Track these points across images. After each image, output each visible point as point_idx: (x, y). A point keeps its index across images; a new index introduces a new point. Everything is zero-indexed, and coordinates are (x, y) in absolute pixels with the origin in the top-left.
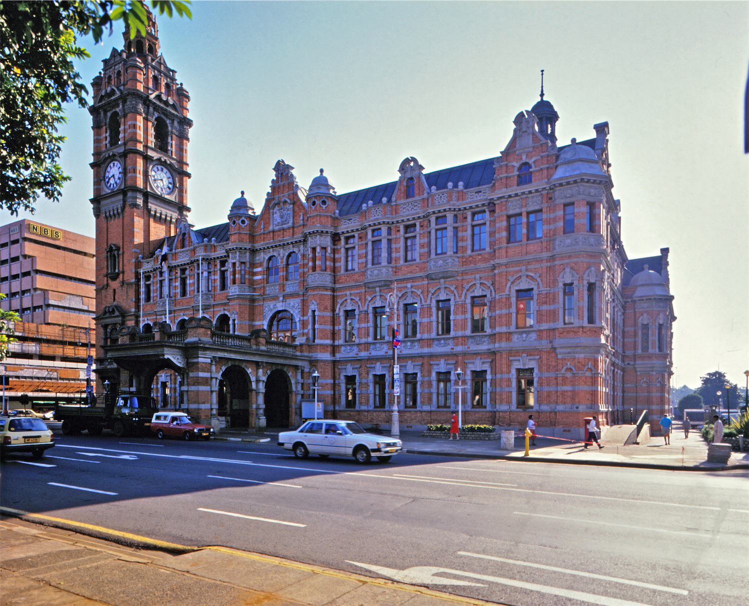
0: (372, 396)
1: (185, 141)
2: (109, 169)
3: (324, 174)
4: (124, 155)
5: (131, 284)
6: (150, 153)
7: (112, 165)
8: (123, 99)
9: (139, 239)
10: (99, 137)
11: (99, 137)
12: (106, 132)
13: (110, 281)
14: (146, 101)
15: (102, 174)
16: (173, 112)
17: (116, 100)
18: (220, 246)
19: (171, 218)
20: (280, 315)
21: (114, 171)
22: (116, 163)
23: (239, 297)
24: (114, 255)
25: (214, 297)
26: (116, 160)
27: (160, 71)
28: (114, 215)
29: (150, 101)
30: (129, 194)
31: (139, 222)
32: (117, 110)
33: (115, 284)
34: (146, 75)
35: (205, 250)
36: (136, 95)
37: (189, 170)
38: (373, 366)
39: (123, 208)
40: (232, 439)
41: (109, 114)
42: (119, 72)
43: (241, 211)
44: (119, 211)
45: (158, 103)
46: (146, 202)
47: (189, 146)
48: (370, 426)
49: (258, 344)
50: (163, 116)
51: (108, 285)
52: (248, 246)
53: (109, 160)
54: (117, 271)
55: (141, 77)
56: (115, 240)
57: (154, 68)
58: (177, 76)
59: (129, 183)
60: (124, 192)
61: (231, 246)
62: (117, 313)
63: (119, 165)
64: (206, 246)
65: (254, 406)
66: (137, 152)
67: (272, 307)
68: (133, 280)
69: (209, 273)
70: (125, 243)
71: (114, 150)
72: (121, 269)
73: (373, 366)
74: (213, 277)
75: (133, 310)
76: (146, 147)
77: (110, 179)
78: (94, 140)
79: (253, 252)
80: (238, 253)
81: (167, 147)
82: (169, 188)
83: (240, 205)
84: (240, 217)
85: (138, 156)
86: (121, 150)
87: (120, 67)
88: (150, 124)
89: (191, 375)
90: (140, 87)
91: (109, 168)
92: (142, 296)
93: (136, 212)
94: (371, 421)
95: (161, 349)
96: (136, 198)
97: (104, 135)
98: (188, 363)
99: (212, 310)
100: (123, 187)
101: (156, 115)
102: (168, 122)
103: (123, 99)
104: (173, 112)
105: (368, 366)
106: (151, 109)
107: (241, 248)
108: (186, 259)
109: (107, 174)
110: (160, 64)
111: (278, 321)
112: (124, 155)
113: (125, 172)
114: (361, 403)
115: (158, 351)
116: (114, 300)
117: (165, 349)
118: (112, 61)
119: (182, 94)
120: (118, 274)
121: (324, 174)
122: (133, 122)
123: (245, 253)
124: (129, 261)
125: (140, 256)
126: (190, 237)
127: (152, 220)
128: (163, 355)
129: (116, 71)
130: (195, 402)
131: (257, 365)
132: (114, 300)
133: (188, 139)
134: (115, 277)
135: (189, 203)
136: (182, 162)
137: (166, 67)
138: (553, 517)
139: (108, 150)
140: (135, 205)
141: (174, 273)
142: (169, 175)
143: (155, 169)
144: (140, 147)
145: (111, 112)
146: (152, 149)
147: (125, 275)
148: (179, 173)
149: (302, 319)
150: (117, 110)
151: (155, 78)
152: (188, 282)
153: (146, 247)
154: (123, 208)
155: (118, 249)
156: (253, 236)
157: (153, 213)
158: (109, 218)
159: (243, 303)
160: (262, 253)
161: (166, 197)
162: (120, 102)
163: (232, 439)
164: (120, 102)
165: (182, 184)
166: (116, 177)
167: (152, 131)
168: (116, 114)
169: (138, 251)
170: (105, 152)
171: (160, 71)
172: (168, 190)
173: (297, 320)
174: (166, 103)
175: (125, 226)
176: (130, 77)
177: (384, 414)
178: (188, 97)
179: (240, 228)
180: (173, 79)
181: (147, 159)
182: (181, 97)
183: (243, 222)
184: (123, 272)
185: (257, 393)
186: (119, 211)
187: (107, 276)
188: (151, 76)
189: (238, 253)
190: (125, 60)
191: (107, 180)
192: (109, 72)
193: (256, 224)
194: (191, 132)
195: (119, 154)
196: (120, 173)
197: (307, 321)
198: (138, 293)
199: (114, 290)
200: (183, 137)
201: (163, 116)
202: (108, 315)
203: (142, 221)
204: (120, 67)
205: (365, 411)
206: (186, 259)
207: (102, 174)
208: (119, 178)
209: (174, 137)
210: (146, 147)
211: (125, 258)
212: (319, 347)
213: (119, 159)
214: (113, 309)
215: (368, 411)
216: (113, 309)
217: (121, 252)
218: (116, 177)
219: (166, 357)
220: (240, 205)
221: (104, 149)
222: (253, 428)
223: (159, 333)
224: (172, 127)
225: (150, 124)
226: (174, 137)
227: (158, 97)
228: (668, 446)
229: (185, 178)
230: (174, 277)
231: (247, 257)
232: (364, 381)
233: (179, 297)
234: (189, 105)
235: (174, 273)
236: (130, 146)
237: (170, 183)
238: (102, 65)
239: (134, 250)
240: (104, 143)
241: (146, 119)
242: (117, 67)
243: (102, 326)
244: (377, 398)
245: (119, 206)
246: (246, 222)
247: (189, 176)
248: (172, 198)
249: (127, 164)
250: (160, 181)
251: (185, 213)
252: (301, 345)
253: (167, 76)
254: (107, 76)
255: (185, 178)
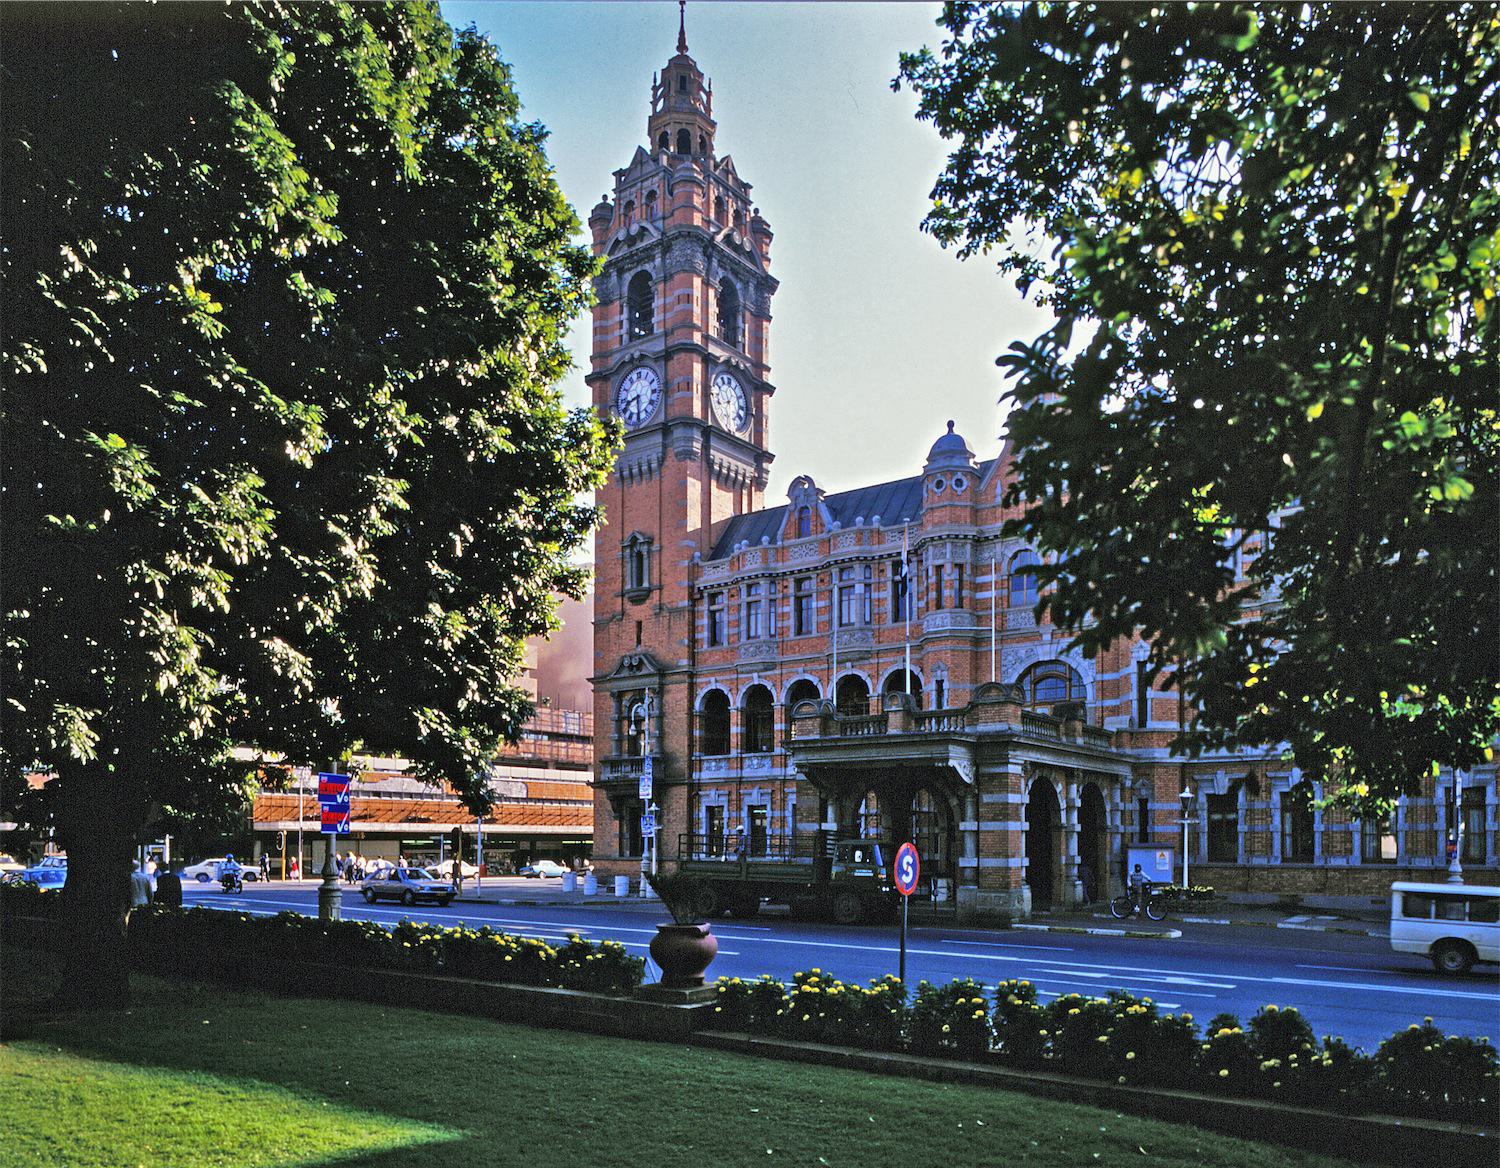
0: (1277, 838)
1: (765, 324)
2: (627, 384)
3: (956, 431)
4: (667, 356)
5: (679, 611)
6: (713, 350)
7: (634, 376)
8: (666, 245)
9: (694, 522)
10: (604, 323)
11: (604, 323)
12: (621, 313)
13: (628, 605)
14: (708, 247)
15: (612, 395)
16: (750, 265)
17: (651, 248)
18: (892, 531)
19: (744, 476)
20: (1039, 671)
21: (641, 388)
22: (644, 372)
23: (953, 636)
24: (640, 555)
25: (878, 634)
26: (644, 366)
27: (727, 188)
28: (631, 475)
29: (714, 246)
30: (678, 433)
31: (694, 488)
32: (648, 267)
33: (638, 612)
34: (706, 195)
35: (859, 541)
36: (692, 235)
37: (770, 378)
38: (1282, 774)
39: (661, 461)
40: (1097, 931)
41: (628, 277)
42: (652, 195)
43: (956, 462)
44: (654, 465)
45: (727, 250)
46: (706, 447)
47: (771, 330)
48: (1276, 899)
49: (1071, 733)
50: (731, 276)
51: (623, 613)
52: (972, 531)
53: (628, 368)
54: (646, 584)
55: (697, 201)
56: (642, 522)
57: (718, 182)
58: (752, 195)
59: (676, 411)
60: (665, 429)
61: (930, 531)
62: (648, 669)
63: (652, 376)
64: (861, 532)
65: (1064, 859)
66: (692, 349)
67: (1022, 653)
68: (686, 603)
69: (867, 586)
70: (664, 530)
71: (644, 347)
72: (656, 582)
73: (1282, 774)
74: (875, 595)
75: (684, 662)
76: (706, 338)
77: (629, 403)
78: (595, 329)
79: (979, 542)
80: (949, 546)
81: (736, 337)
82: (739, 416)
83: (950, 448)
84: (953, 473)
85: (695, 356)
86: (659, 346)
87: (655, 183)
88: (711, 293)
89: (986, 798)
90: (697, 220)
91: (627, 382)
92: (704, 635)
93: (692, 466)
94: (1275, 889)
95: (941, 749)
96: (692, 439)
97: (617, 318)
98: (977, 776)
99: (874, 661)
100: (661, 418)
101: (721, 273)
102: (739, 286)
103: (666, 245)
104: (750, 265)
105: (1270, 774)
106: (715, 263)
107: (957, 536)
108: (816, 558)
109: (623, 395)
110: (727, 172)
111: (1036, 683)
112: (667, 356)
113: (666, 389)
114: (1251, 852)
115: (936, 751)
116: (639, 642)
117: (951, 747)
118: (636, 174)
119: (761, 231)
120: (649, 591)
121: (956, 431)
122: (687, 291)
123: (963, 545)
124: (675, 564)
125: (698, 554)
126: (818, 515)
127: (714, 483)
128: (947, 760)
129: (645, 193)
130: (996, 855)
131: (1069, 774)
132: (639, 642)
133: (769, 319)
134: (639, 598)
135: (770, 444)
136: (761, 367)
137: (736, 179)
138: (970, 1067)
139: (627, 348)
140: (688, 454)
141: (779, 587)
142: (739, 391)
143: (719, 381)
144: (697, 338)
145: (633, 273)
146: (715, 341)
147: (665, 593)
148: (755, 387)
149: (1099, 677)
150: (648, 267)
151: (719, 202)
152: (814, 604)
153: (705, 536)
154: (661, 461)
155: (650, 542)
156: (977, 511)
157: (716, 468)
158: (627, 481)
159: (960, 646)
160: (998, 546)
161: (738, 435)
162: (658, 252)
163: (1097, 931)
164: (658, 252)
165: (759, 408)
166: (645, 401)
167: (714, 309)
168: (644, 277)
169: (693, 544)
170: (617, 351)
171: (727, 188)
172: (738, 421)
173: (1087, 680)
174: (738, 249)
175: (665, 496)
176: (677, 204)
177: (1310, 875)
178: (770, 236)
179: (954, 493)
180: (747, 202)
181: (708, 360)
182: (759, 236)
183: (959, 483)
184: (661, 588)
185: (1069, 834)
186: (654, 465)
187: (623, 596)
188: (713, 197)
189: (949, 546)
190: (665, 170)
191: (623, 406)
192: (630, 194)
193: (982, 487)
194: (776, 302)
195: (654, 353)
196: (654, 391)
197: (1127, 677)
198: (693, 629)
199: (639, 624)
200: (762, 315)
201: (731, 276)
202: (625, 673)
203: (698, 485)
204: (655, 183)
205: (1263, 868)
206: (816, 558)
207: (612, 395)
208: (651, 402)
209: (748, 314)
210: (706, 338)
211: (664, 558)
212: (1155, 736)
213: (652, 364)
214: (641, 662)
215: (1270, 869)
216: (641, 662)
217: (655, 547)
218: (645, 401)
219: (951, 763)
220: (950, 448)
221: (617, 346)
222: (1061, 904)
223: (899, 716)
224: (745, 298)
225: (711, 293)
226: (748, 314)
227: (728, 239)
228: (634, 898)
229: (765, 397)
230: (780, 596)
231: (966, 555)
232: (1259, 805)
233: (792, 635)
234: (772, 250)
235: (779, 587)
236: (678, 338)
237: (741, 408)
238: (612, 182)
239: (686, 542)
240: (617, 333)
241: (706, 284)
242: (645, 184)
243: (612, 695)
244: (1288, 840)
245: (654, 456)
246: (966, 483)
247: (770, 390)
248: (744, 436)
249: (670, 373)
250: (727, 408)
251: (765, 465)
252: (1119, 733)
253: (737, 197)
254: (623, 203)
255: (765, 397)
